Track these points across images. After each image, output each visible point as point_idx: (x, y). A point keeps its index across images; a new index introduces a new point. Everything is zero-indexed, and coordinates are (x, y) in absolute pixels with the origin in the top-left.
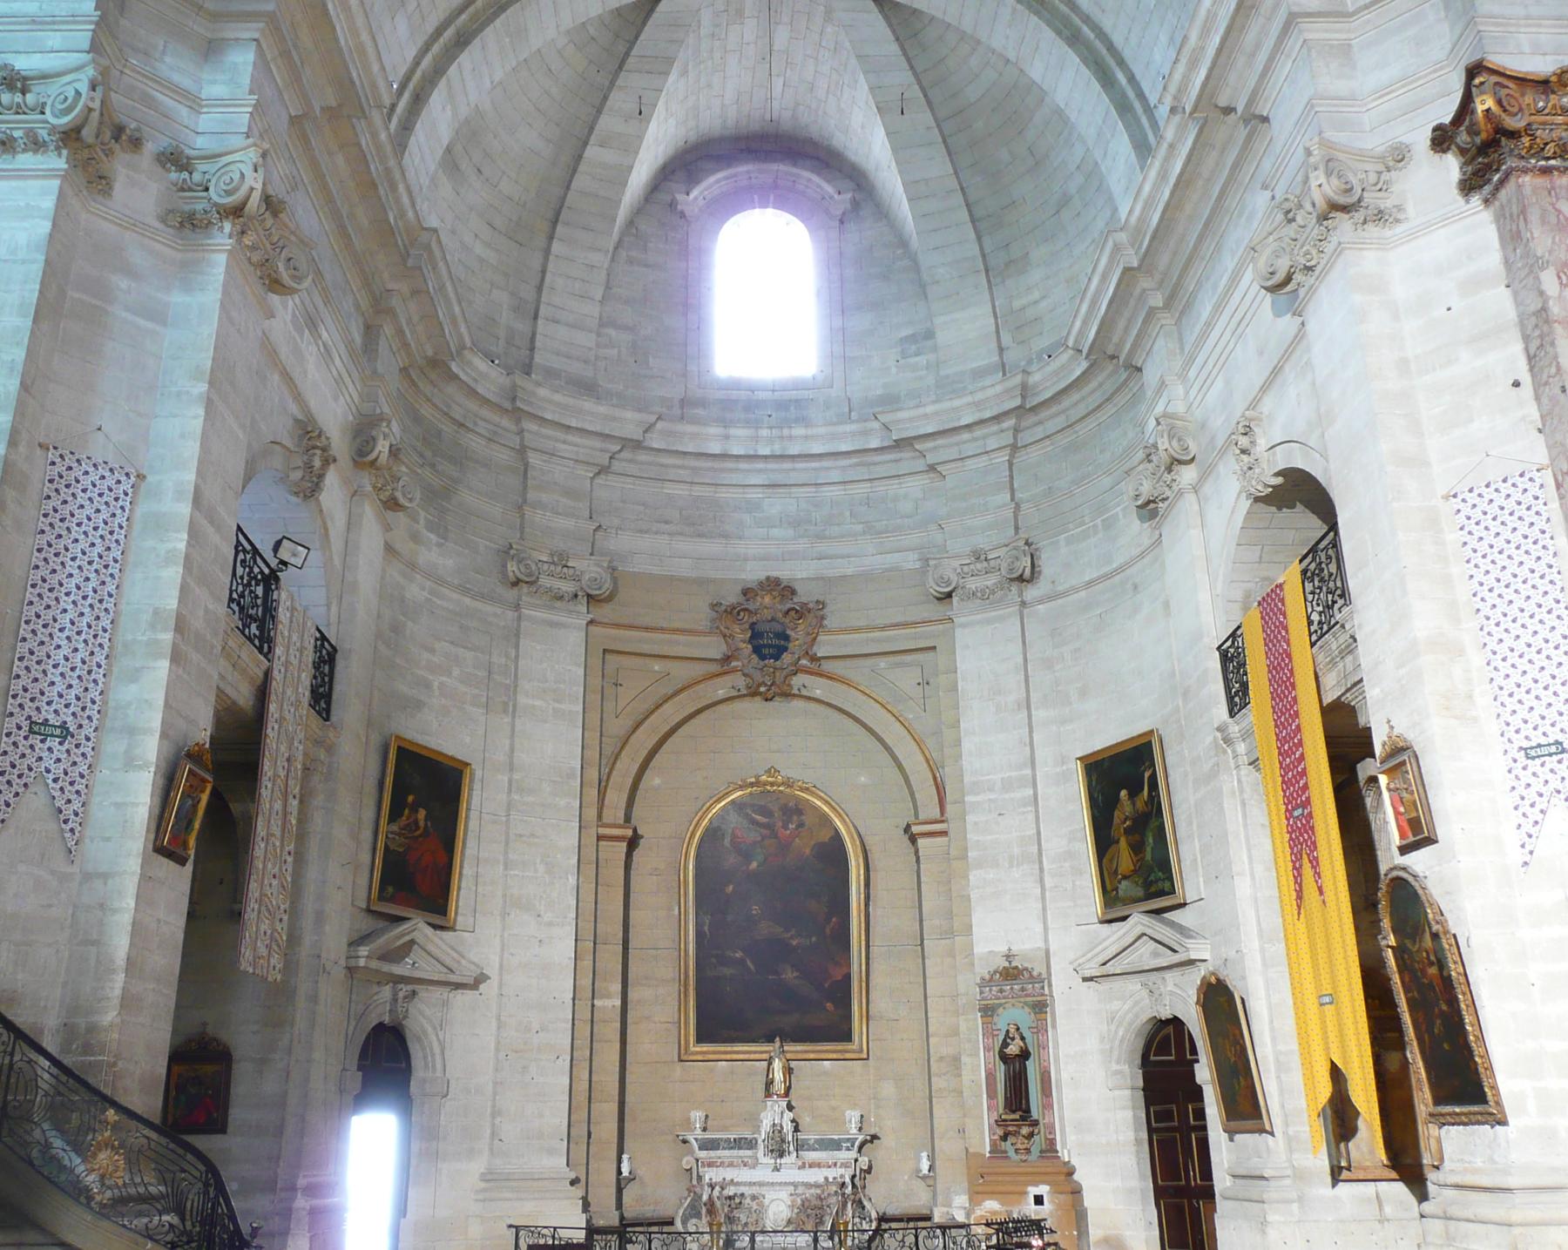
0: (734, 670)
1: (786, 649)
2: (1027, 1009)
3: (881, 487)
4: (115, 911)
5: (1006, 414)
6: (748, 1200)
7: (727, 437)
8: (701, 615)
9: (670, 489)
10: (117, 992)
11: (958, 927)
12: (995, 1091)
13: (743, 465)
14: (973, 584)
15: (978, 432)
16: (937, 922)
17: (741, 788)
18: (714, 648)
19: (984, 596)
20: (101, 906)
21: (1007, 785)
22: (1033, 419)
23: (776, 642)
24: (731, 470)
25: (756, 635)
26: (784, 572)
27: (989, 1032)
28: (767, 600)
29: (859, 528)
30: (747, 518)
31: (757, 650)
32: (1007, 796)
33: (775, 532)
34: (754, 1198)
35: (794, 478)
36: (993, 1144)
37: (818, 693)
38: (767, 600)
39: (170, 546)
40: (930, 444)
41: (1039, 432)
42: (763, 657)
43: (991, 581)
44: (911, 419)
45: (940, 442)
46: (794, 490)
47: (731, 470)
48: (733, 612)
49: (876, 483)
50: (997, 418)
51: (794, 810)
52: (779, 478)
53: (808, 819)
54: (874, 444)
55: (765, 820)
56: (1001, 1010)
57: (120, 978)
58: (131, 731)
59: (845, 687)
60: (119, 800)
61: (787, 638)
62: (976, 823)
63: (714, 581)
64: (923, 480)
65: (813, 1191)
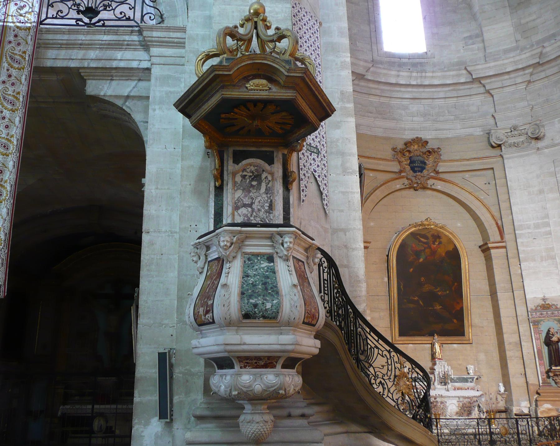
0: (403, 177)
1: (424, 168)
2: (556, 322)
3: (461, 100)
4: (353, 249)
5: (529, 66)
6: (439, 404)
7: (398, 76)
8: (389, 154)
9: (372, 99)
10: (364, 293)
11: (516, 286)
12: (542, 357)
13: (403, 89)
14: (512, 140)
15: (513, 75)
16: (502, 285)
17: (415, 226)
18: (396, 167)
19: (515, 145)
20: (346, 246)
21: (537, 226)
22: (540, 69)
23: (421, 165)
24: (398, 91)
25: (412, 162)
26: (425, 136)
27: (538, 332)
28: (416, 147)
29: (452, 117)
30: (403, 112)
31: (413, 169)
32: (537, 231)
33: (415, 119)
34: (442, 403)
35: (424, 95)
36: (543, 380)
37: (439, 188)
38: (416, 147)
39: (343, 60)
40: (488, 81)
41: (543, 75)
42: (415, 172)
43: (522, 138)
44: (482, 69)
45: (493, 80)
46: (423, 101)
47: (398, 91)
48: (402, 152)
49: (459, 98)
50: (523, 69)
51: (437, 237)
52: (417, 95)
53: (444, 240)
54: (463, 80)
55: (426, 241)
56: (542, 323)
57: (364, 286)
58: (343, 154)
59: (451, 185)
60: (343, 190)
61: (425, 163)
62: (522, 243)
63: (392, 138)
64: (481, 97)
65: (467, 400)
